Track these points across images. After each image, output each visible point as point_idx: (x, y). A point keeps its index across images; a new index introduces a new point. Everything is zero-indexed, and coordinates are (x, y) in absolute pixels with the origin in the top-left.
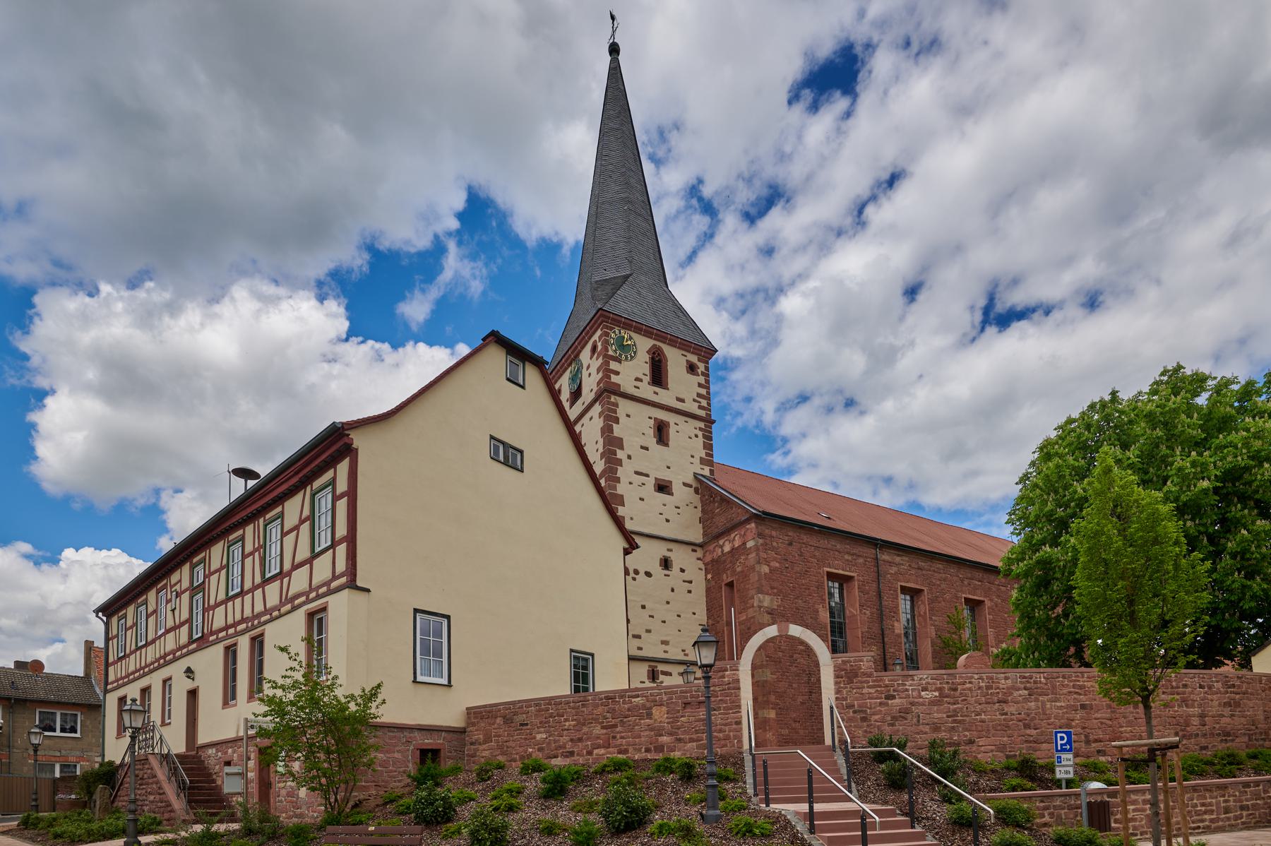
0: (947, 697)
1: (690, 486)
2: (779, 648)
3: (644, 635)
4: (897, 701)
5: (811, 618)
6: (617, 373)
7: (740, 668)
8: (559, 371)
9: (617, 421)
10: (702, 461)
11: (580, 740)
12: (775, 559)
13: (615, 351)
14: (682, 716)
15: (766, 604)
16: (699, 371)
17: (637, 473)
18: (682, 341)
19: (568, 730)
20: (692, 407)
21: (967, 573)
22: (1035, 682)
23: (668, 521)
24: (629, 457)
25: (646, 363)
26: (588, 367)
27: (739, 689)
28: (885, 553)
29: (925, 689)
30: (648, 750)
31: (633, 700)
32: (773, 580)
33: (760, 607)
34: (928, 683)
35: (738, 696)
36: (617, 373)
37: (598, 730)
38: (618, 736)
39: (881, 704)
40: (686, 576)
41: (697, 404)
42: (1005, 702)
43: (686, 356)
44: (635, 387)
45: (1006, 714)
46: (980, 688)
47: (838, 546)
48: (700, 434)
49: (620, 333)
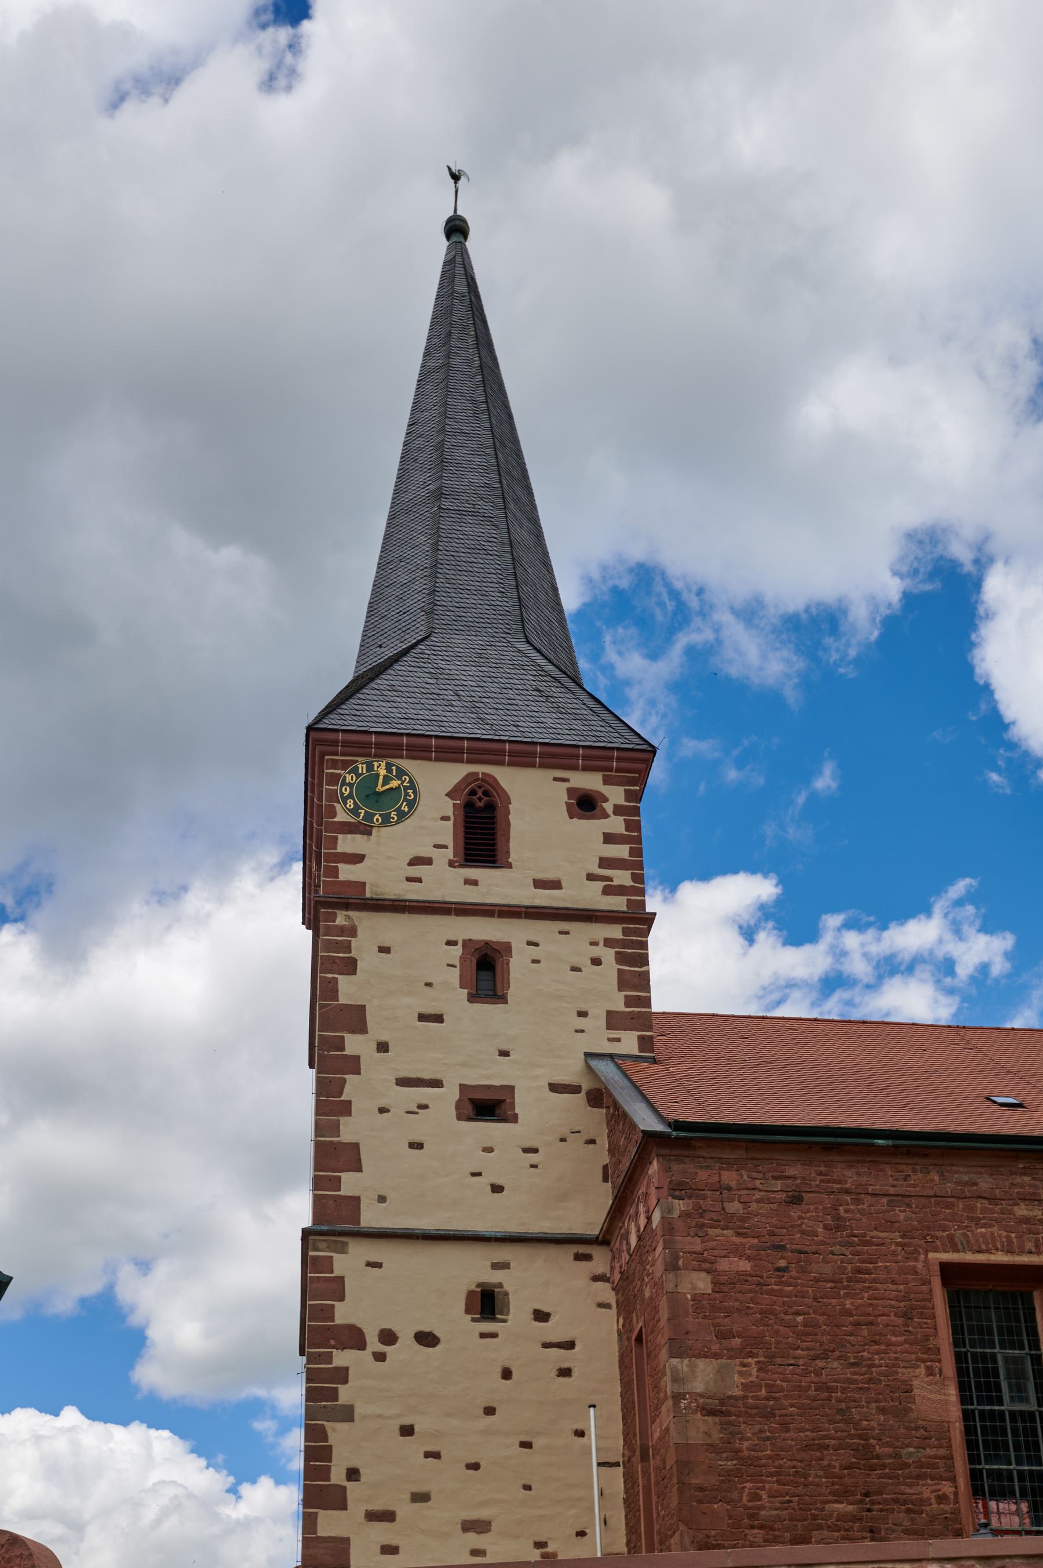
1: (575, 1089)
2: (751, 1516)
3: (405, 1510)
5: (882, 1411)
9: (350, 967)
10: (613, 1020)
12: (738, 1252)
13: (355, 811)
15: (698, 1386)
16: (608, 807)
17: (404, 1082)
18: (442, 742)
20: (592, 897)
23: (497, 1189)
24: (383, 1047)
25: (445, 818)
32: (729, 1313)
36: (358, 858)
40: (552, 1331)
41: (600, 885)
44: (409, 879)
47: (985, 1183)
48: (608, 955)
49: (370, 767)
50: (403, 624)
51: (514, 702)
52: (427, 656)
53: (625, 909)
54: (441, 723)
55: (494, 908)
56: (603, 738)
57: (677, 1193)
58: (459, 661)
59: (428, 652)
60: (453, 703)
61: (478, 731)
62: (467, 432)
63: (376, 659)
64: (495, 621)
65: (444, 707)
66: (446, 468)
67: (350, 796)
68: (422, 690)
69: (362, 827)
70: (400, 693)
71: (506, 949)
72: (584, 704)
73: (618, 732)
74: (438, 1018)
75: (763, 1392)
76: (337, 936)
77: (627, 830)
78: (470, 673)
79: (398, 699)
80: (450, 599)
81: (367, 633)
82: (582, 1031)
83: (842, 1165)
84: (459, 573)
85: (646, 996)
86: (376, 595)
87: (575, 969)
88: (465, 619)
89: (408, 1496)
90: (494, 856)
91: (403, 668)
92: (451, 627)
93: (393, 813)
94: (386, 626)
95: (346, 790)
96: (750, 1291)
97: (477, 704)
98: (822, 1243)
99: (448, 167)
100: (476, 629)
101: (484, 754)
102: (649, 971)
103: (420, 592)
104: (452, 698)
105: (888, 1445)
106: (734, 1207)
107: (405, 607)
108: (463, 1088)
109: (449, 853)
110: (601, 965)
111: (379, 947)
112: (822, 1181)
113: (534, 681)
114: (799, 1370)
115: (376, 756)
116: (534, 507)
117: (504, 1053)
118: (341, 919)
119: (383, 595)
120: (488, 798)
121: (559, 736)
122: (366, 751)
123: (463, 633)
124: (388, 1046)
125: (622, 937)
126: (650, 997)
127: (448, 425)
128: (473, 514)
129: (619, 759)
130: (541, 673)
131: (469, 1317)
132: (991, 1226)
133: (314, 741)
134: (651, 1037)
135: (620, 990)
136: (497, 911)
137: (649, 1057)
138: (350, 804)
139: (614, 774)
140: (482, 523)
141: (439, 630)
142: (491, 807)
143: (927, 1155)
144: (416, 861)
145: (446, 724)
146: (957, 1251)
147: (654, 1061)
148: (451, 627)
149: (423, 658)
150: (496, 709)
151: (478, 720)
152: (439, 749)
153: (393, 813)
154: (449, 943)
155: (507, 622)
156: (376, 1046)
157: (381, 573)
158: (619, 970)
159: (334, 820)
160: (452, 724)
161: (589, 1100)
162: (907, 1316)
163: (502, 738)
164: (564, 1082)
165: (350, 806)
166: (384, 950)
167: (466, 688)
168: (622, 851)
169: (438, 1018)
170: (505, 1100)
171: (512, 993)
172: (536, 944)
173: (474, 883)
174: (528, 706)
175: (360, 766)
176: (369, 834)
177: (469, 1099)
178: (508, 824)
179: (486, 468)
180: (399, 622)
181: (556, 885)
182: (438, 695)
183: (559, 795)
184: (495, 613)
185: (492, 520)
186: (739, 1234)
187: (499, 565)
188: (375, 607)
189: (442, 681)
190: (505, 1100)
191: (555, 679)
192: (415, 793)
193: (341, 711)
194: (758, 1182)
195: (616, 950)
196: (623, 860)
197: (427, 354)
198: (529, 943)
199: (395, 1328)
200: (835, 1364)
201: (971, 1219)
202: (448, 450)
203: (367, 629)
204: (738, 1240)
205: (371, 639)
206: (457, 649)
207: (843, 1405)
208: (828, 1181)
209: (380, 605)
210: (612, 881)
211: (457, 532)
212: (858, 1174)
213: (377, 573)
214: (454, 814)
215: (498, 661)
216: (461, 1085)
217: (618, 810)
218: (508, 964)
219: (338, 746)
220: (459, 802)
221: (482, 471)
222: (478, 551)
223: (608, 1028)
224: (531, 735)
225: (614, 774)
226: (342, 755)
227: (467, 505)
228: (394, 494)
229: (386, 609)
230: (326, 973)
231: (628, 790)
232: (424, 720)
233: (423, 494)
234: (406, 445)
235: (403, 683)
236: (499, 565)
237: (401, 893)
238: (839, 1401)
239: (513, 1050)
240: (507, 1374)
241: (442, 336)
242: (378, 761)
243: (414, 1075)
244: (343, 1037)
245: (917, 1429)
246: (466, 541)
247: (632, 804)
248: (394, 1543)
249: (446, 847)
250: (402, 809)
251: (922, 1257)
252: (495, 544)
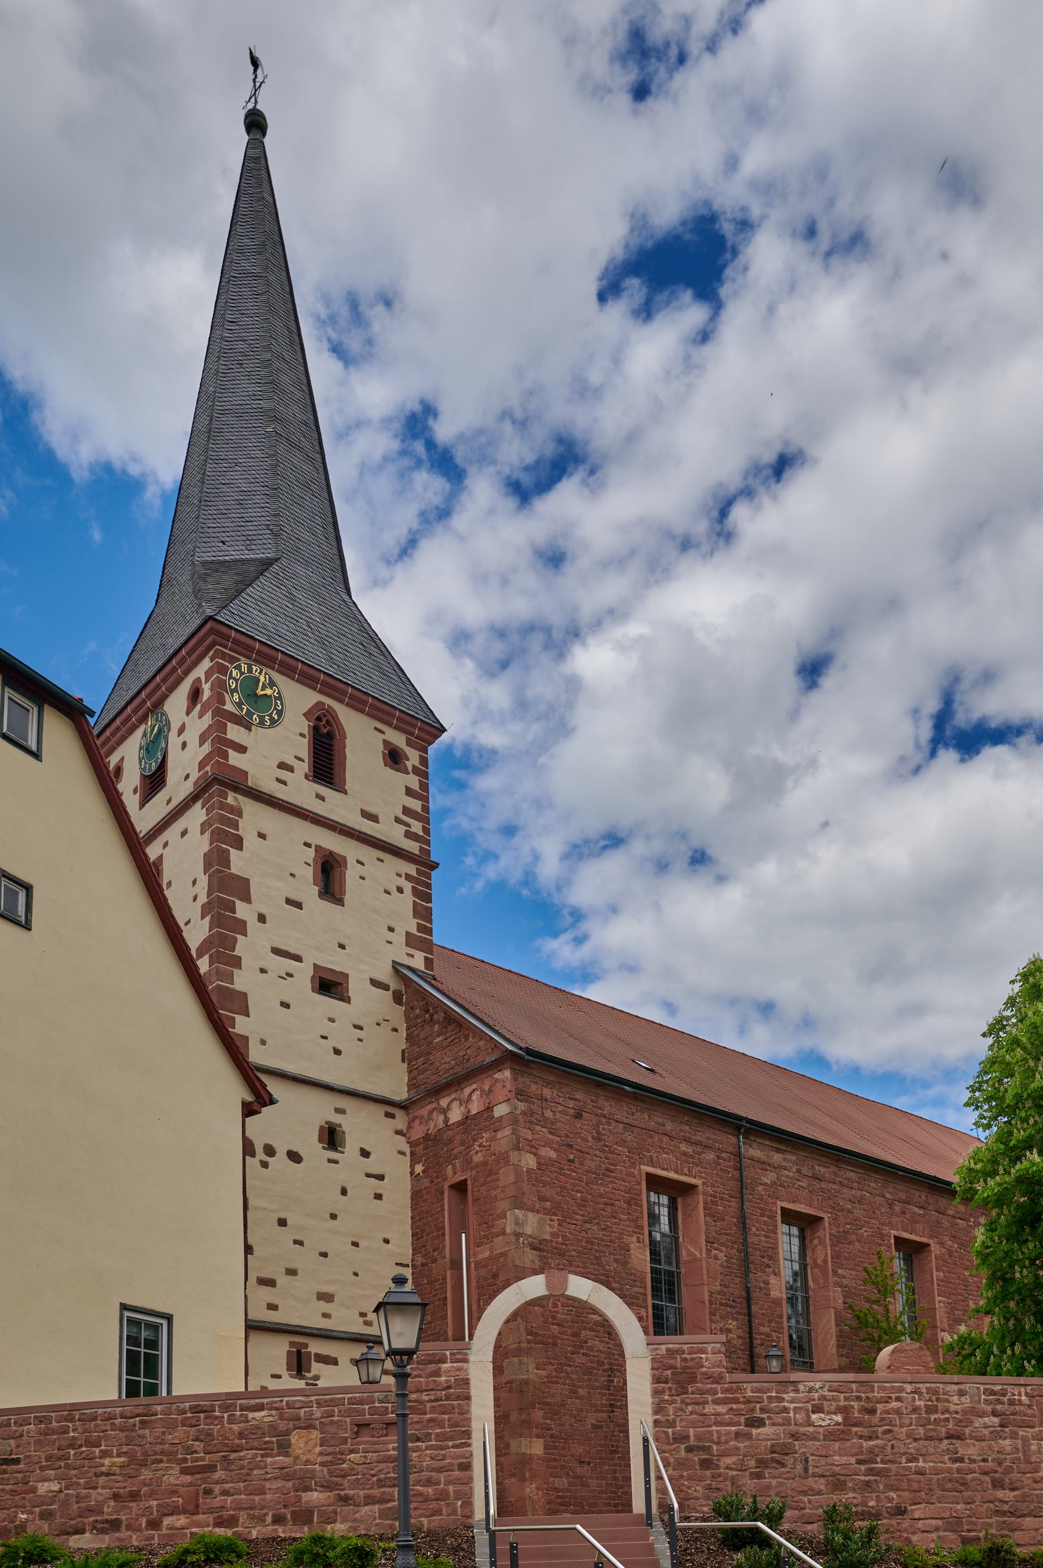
0: (857, 1424)
3: (282, 1280)
4: (767, 1430)
5: (616, 1260)
6: (242, 749)
7: (472, 1358)
8: (118, 729)
11: (134, 1496)
12: (548, 1144)
13: (239, 705)
14: (352, 1452)
16: (409, 765)
17: (277, 951)
19: (108, 1475)
20: (396, 835)
21: (894, 1191)
22: (1011, 1402)
23: (337, 1052)
24: (262, 918)
25: (302, 735)
26: (181, 730)
27: (468, 1398)
28: (755, 1145)
29: (818, 1409)
30: (278, 1520)
31: (251, 1415)
33: (517, 1235)
34: (823, 1398)
35: (465, 1412)
36: (242, 749)
37: (173, 1477)
38: (217, 1489)
39: (737, 1435)
40: (372, 1165)
42: (960, 1437)
43: (382, 732)
45: (961, 1460)
46: (915, 1410)
47: (669, 1127)
48: (408, 887)
57: (519, 1097)
75: (560, 1240)
82: (391, 943)
83: (603, 1098)
89: (284, 1270)
96: (556, 1172)
98: (591, 1148)
105: (618, 1282)
106: (548, 1114)
112: (593, 1106)
114: (578, 1228)
115: (254, 660)
118: (231, 798)
129: (420, 729)
131: (321, 1145)
132: (669, 1154)
134: (432, 959)
142: (330, 735)
143: (643, 1101)
146: (653, 1167)
152: (302, 674)
162: (628, 1203)
186: (550, 1133)
190: (342, 984)
192: (282, 704)
194: (561, 1099)
199: (275, 1145)
200: (595, 1228)
201: (661, 1148)
204: (550, 1136)
207: (598, 1254)
208: (596, 1107)
212: (610, 1106)
226: (229, 650)
238: (596, 1251)
240: (344, 1192)
245: (631, 1274)
248: (275, 1302)
251: (637, 1167)
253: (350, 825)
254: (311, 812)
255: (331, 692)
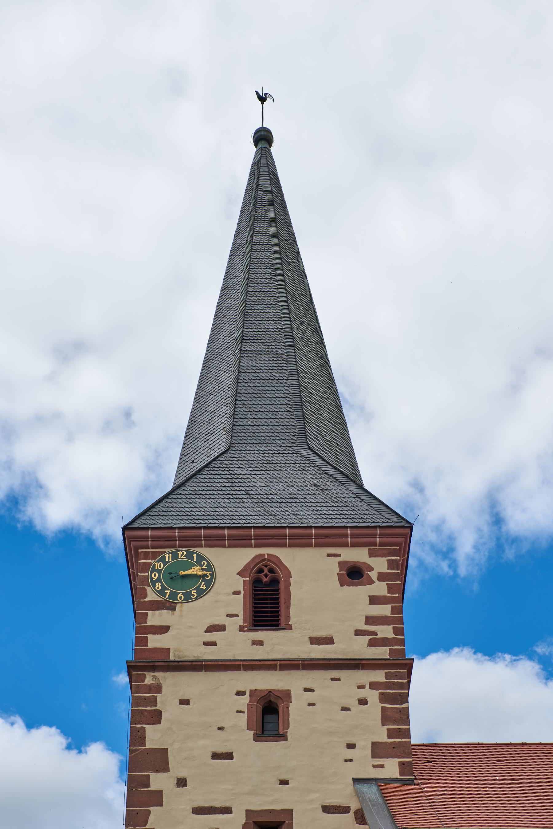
1: (345, 810)
13: (162, 592)
16: (373, 575)
25: (237, 593)
36: (164, 629)
41: (366, 638)
44: (206, 644)
48: (373, 696)
49: (175, 556)
50: (210, 443)
51: (295, 496)
52: (225, 466)
53: (388, 657)
54: (233, 517)
55: (276, 662)
56: (367, 520)
58: (252, 467)
59: (226, 462)
60: (244, 500)
61: (264, 521)
62: (266, 290)
63: (189, 472)
64: (283, 434)
65: (236, 504)
66: (248, 319)
67: (159, 580)
68: (219, 492)
69: (168, 605)
70: (201, 496)
71: (287, 695)
72: (354, 494)
73: (380, 514)
74: (229, 756)
76: (145, 693)
77: (389, 592)
78: (260, 476)
79: (199, 501)
80: (246, 420)
81: (184, 453)
82: (351, 760)
84: (255, 399)
85: (406, 729)
86: (192, 423)
87: (345, 709)
88: (258, 435)
90: (278, 621)
91: (205, 476)
92: (246, 442)
93: (193, 591)
94: (198, 445)
95: (155, 575)
97: (264, 500)
99: (256, 91)
100: (267, 441)
101: (268, 539)
102: (408, 708)
103: (223, 416)
104: (244, 496)
107: (212, 429)
108: (249, 813)
109: (240, 621)
110: (367, 704)
111: (180, 700)
113: (313, 478)
115: (180, 546)
116: (323, 345)
117: (284, 782)
118: (149, 679)
119: (197, 422)
120: (273, 574)
121: (331, 521)
122: (172, 543)
123: (256, 446)
124: (186, 781)
125: (385, 680)
126: (409, 729)
127: (250, 286)
128: (268, 353)
129: (381, 535)
130: (319, 472)
133: (129, 538)
135: (383, 724)
136: (278, 665)
137: (409, 780)
138: (158, 586)
139: (378, 548)
140: (275, 359)
141: (237, 445)
142: (275, 581)
144: (212, 629)
145: (237, 517)
147: (412, 782)
148: (246, 442)
149: (222, 467)
150: (280, 503)
151: (263, 512)
153: (193, 591)
154: (238, 693)
155: (292, 434)
156: (176, 782)
157: (196, 405)
158: (382, 708)
159: (145, 600)
160: (242, 517)
161: (356, 819)
163: (283, 525)
164: (335, 804)
165: (158, 588)
166: (185, 702)
167: (255, 488)
168: (385, 610)
169: (229, 756)
170: (285, 822)
171: (290, 733)
172: (312, 690)
173: (261, 643)
174: (306, 498)
175: (167, 555)
176: (174, 609)
177: (253, 822)
178: (289, 594)
179: (279, 317)
180: (207, 442)
181: (329, 641)
182: (232, 495)
183: (333, 566)
184: (283, 428)
185: (283, 356)
187: (288, 390)
188: (191, 432)
189: (237, 485)
191: (331, 476)
193: (151, 513)
195: (380, 691)
196: (386, 617)
197: (237, 234)
198: (306, 690)
202: (249, 306)
203: (184, 449)
205: (186, 457)
206: (250, 459)
209: (194, 430)
210: (377, 635)
211: (254, 368)
213: (194, 405)
214: (244, 588)
215: (283, 465)
216: (247, 811)
217: (382, 577)
218: (288, 708)
219: (149, 541)
220: (248, 579)
221: (276, 319)
222: (271, 381)
223: (373, 757)
224: (307, 521)
225: (378, 548)
226: (152, 548)
227: (263, 346)
228: (208, 344)
229: (199, 433)
230: (136, 724)
231: (390, 560)
232: (218, 515)
233: (229, 341)
234: (219, 306)
235: (204, 488)
236: (288, 390)
237: (199, 655)
239: (292, 779)
241: (248, 220)
242: (181, 551)
243: (207, 805)
244: (149, 776)
246: (261, 374)
247: (393, 571)
249: (237, 616)
250: (201, 587)
252: (285, 375)
253: (296, 657)
254: (241, 660)
255: (270, 541)
